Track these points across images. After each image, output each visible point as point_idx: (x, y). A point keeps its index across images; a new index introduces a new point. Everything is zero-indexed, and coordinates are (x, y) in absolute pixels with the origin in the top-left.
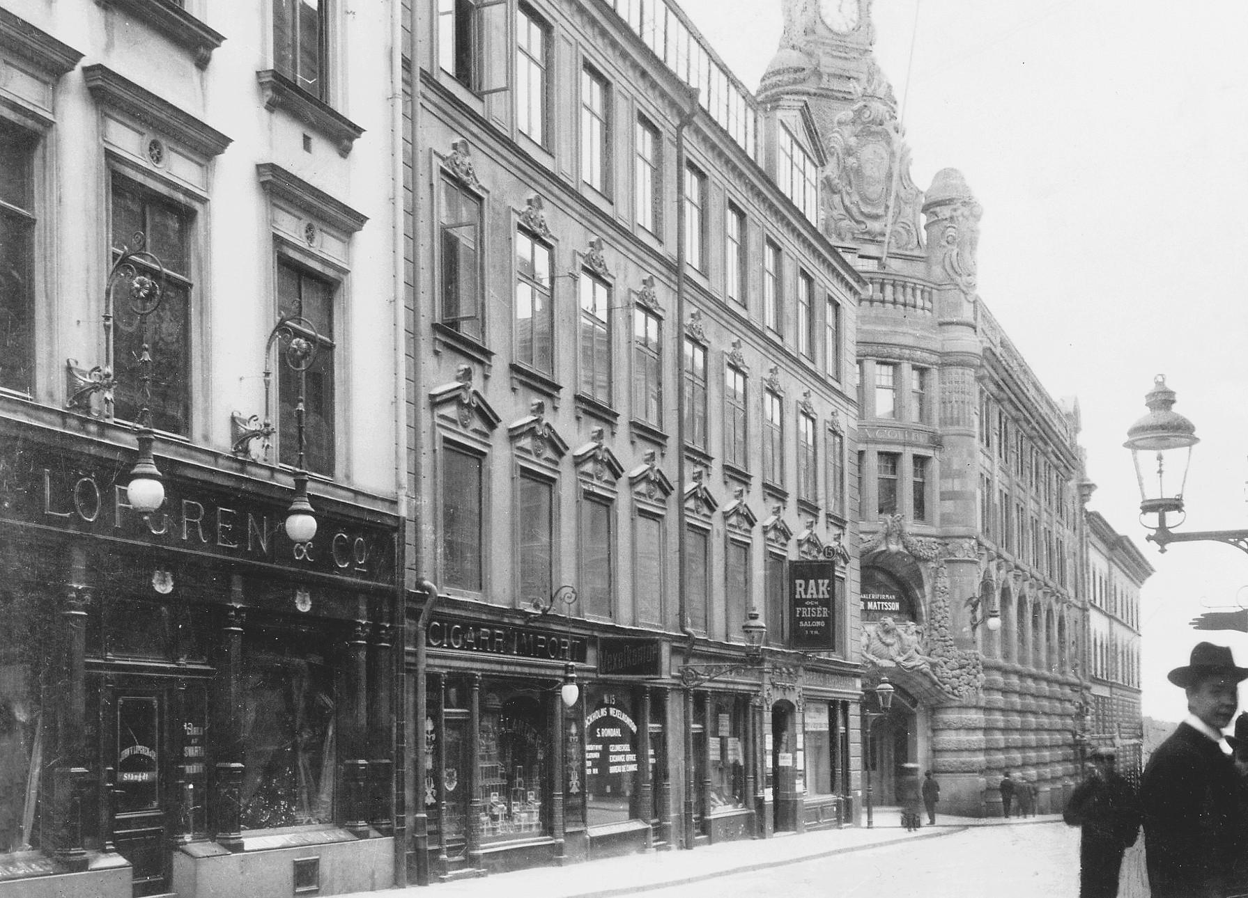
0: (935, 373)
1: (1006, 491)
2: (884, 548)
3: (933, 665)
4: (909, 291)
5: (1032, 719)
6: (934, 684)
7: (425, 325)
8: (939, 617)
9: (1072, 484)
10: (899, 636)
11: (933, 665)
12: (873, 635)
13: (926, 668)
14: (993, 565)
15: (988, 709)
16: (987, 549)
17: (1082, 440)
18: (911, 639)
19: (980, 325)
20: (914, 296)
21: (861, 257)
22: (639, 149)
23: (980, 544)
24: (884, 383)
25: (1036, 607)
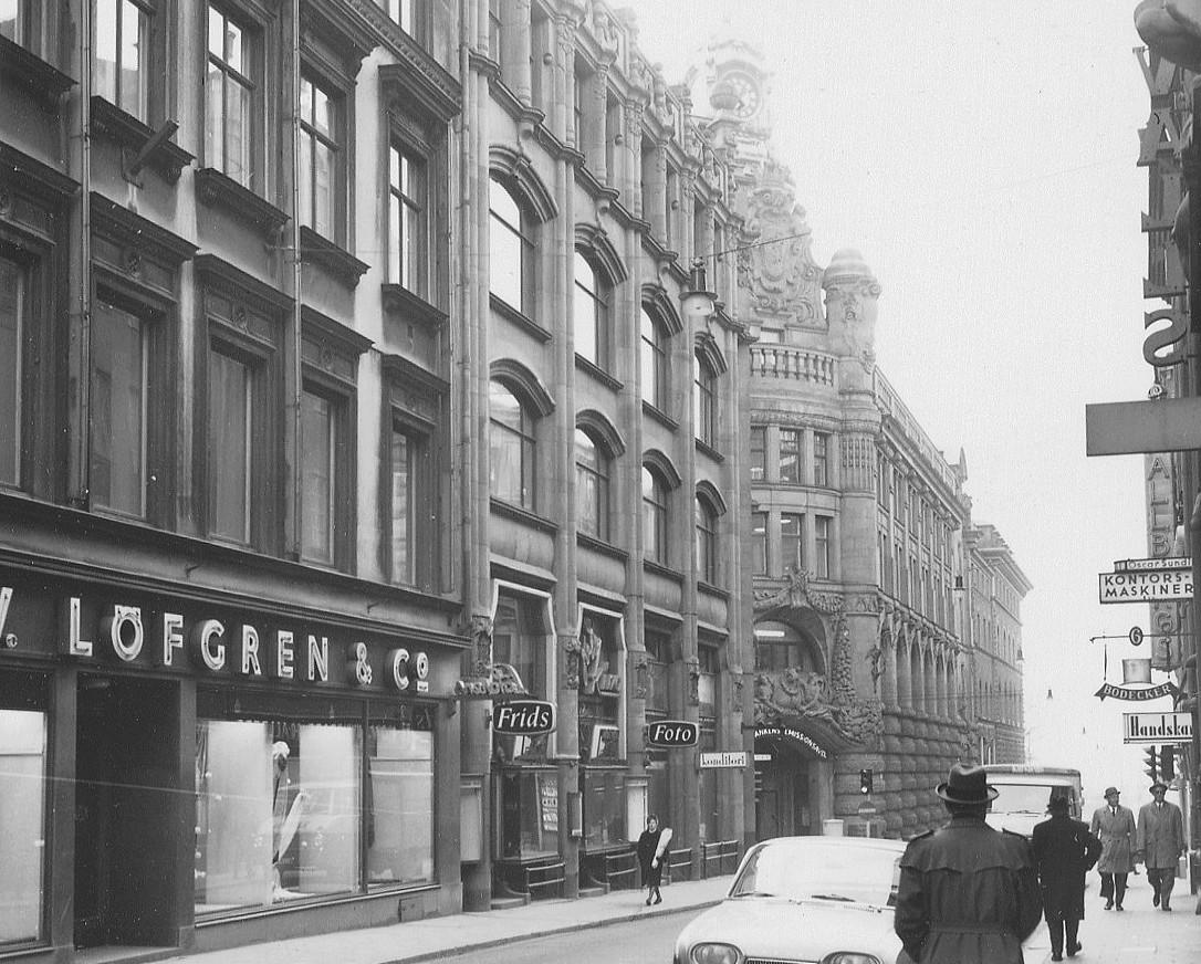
0: (835, 439)
1: (900, 545)
2: (788, 603)
3: (835, 714)
4: (802, 361)
5: (911, 743)
6: (837, 731)
7: (456, 475)
8: (840, 668)
9: (957, 535)
10: (803, 686)
11: (835, 714)
12: (777, 684)
13: (829, 716)
14: (890, 616)
15: (887, 753)
16: (886, 603)
17: (967, 488)
18: (815, 689)
19: (878, 391)
20: (807, 366)
21: (762, 329)
22: (394, 182)
23: (879, 599)
24: (368, 249)
25: (915, 647)
